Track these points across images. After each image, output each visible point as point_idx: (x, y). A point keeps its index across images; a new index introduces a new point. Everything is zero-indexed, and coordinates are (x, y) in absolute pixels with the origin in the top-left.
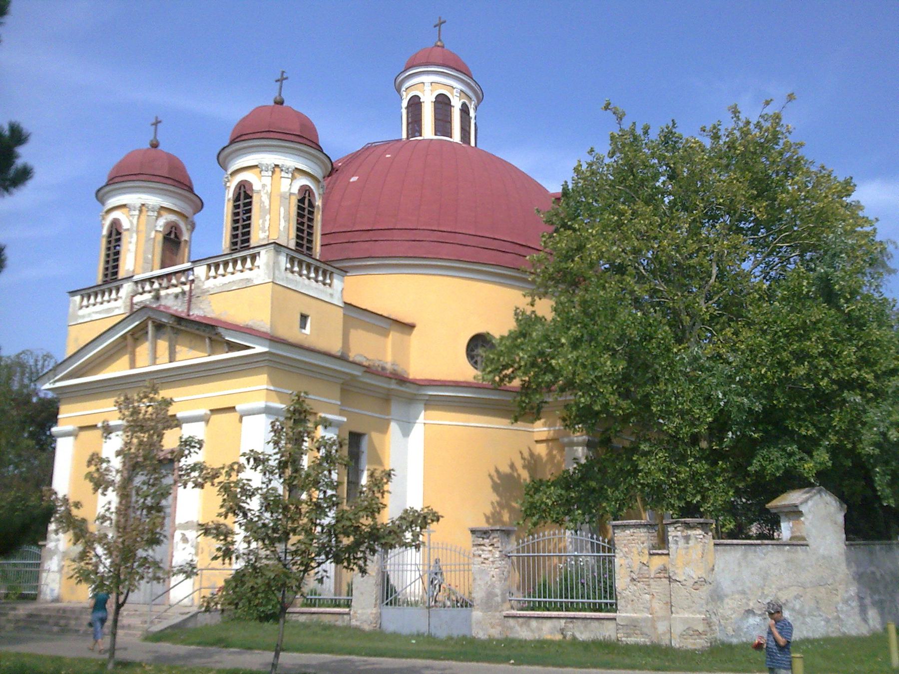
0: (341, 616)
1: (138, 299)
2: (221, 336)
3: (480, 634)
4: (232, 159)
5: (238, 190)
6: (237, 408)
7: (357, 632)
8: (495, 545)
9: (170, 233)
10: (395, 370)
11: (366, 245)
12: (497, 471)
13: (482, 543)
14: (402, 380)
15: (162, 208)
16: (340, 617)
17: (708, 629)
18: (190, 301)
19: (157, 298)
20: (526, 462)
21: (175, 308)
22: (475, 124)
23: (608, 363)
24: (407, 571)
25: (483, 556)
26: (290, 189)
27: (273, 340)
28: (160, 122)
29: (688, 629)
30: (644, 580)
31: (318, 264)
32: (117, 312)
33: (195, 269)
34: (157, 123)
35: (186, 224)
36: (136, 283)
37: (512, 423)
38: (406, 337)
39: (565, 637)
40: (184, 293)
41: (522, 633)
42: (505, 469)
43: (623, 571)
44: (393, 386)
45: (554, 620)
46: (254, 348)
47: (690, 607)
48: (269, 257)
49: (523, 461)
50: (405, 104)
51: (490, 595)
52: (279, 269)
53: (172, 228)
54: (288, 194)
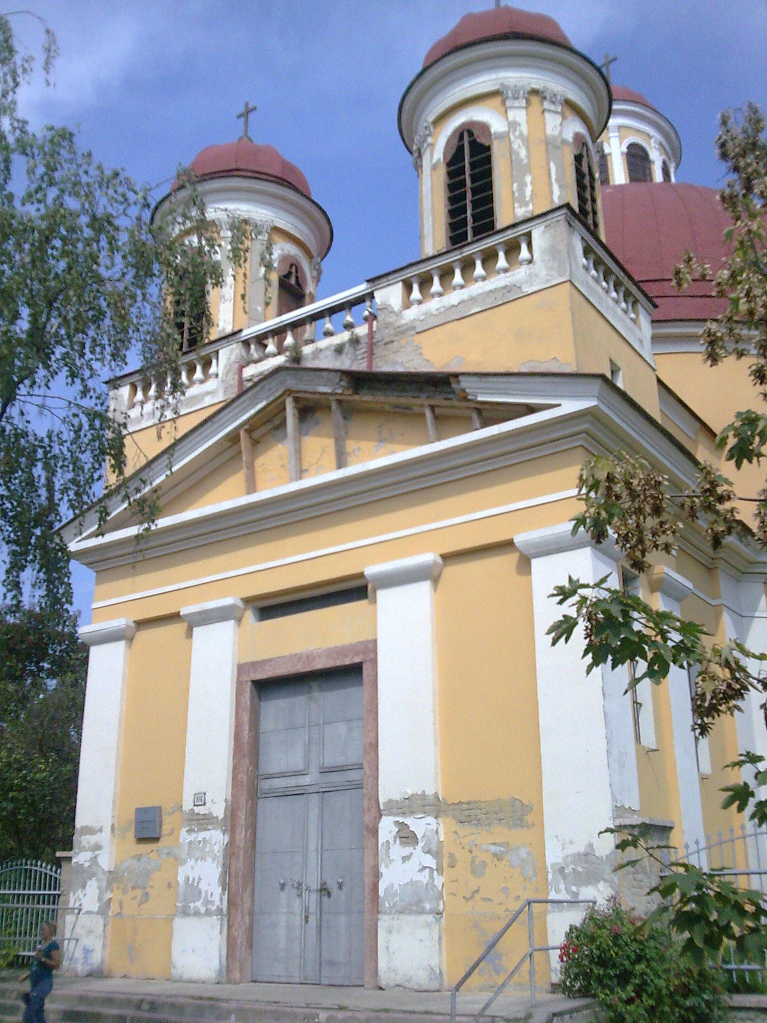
1: (248, 372)
4: (429, 101)
9: (290, 273)
15: (276, 230)
26: (561, 132)
32: (208, 401)
34: (248, 111)
36: (246, 343)
40: (355, 341)
46: (559, 405)
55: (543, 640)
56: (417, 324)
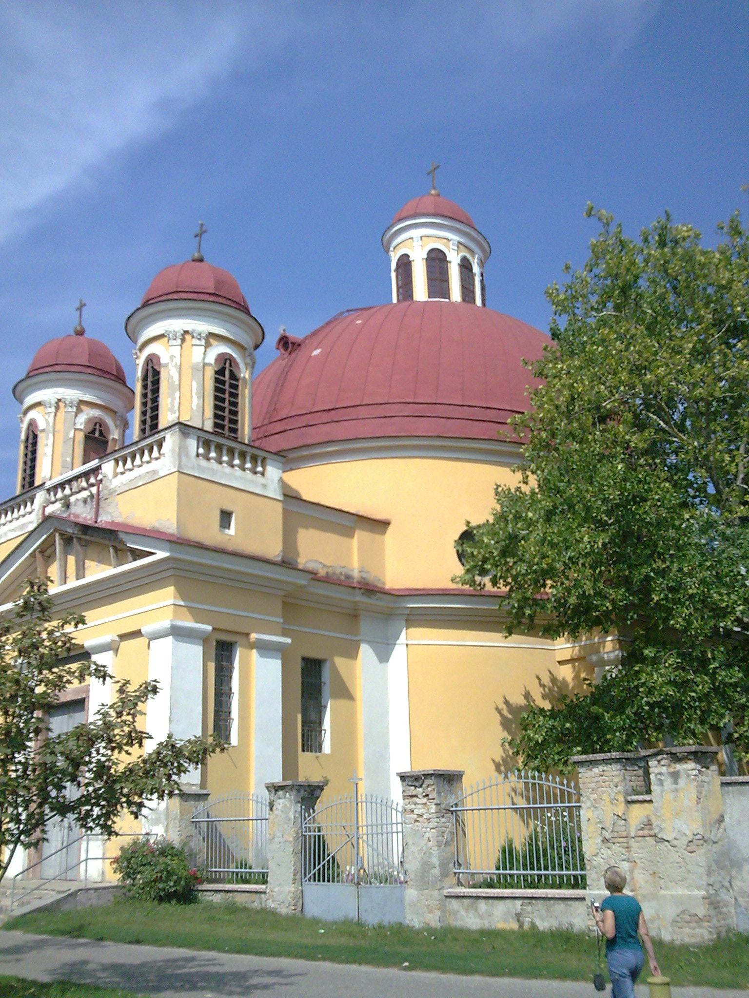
0: (258, 895)
1: (49, 510)
2: (122, 542)
3: (414, 920)
5: (146, 366)
6: (143, 631)
7: (269, 917)
8: (430, 797)
9: (94, 430)
10: (364, 579)
11: (326, 428)
12: (507, 702)
13: (414, 793)
14: (370, 589)
16: (254, 896)
17: (712, 912)
18: (98, 505)
19: (67, 506)
20: (546, 689)
21: (84, 515)
22: (482, 281)
23: (586, 539)
24: (392, 833)
25: (416, 811)
26: (204, 359)
27: (176, 542)
28: (85, 305)
29: (683, 912)
30: (622, 839)
31: (244, 448)
33: (103, 466)
35: (115, 421)
36: (49, 490)
37: (506, 637)
38: (382, 537)
39: (521, 926)
40: (92, 496)
41: (467, 920)
42: (519, 700)
43: (591, 829)
44: (359, 598)
45: (508, 901)
47: (684, 879)
48: (174, 441)
49: (542, 689)
50: (393, 266)
51: (426, 866)
52: (187, 456)
53: (95, 425)
54: (201, 365)
55: (164, 687)
56: (117, 489)
